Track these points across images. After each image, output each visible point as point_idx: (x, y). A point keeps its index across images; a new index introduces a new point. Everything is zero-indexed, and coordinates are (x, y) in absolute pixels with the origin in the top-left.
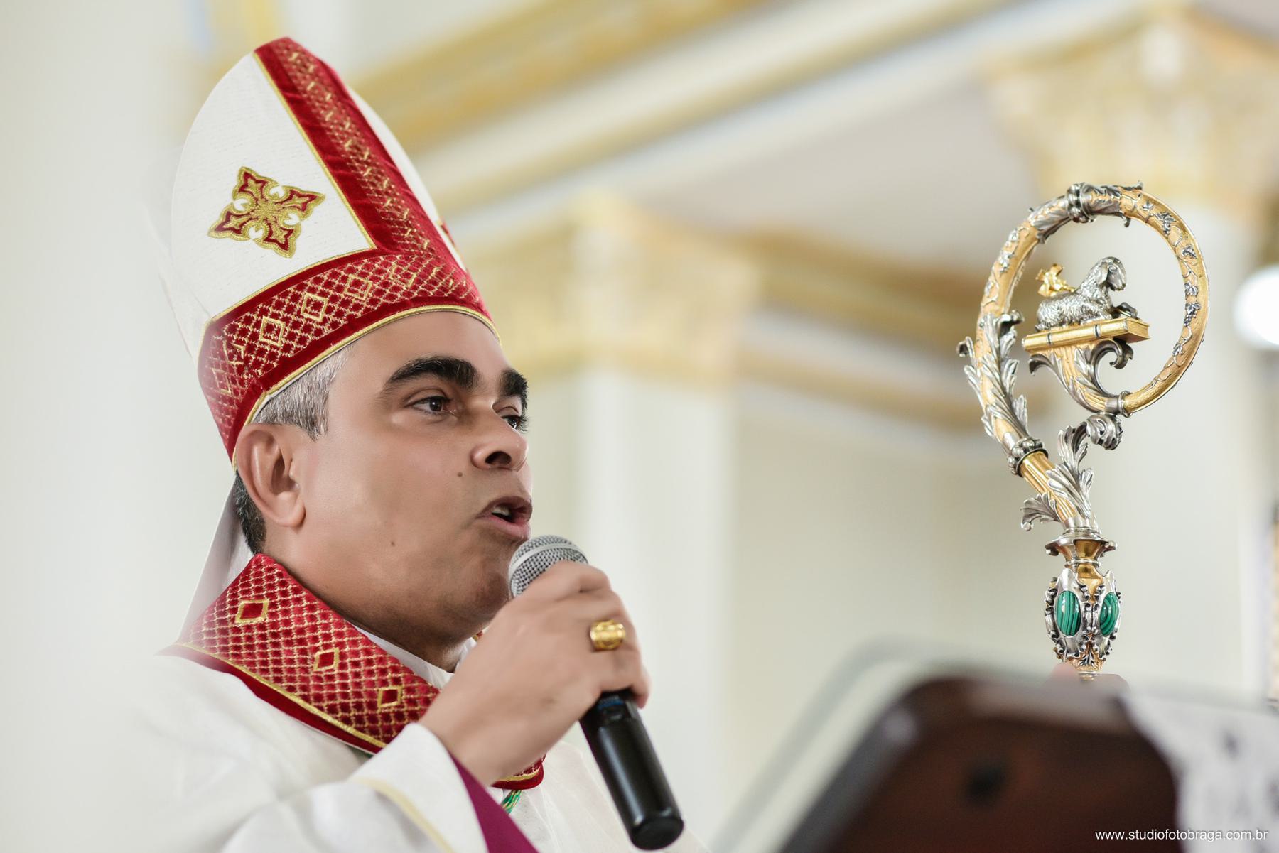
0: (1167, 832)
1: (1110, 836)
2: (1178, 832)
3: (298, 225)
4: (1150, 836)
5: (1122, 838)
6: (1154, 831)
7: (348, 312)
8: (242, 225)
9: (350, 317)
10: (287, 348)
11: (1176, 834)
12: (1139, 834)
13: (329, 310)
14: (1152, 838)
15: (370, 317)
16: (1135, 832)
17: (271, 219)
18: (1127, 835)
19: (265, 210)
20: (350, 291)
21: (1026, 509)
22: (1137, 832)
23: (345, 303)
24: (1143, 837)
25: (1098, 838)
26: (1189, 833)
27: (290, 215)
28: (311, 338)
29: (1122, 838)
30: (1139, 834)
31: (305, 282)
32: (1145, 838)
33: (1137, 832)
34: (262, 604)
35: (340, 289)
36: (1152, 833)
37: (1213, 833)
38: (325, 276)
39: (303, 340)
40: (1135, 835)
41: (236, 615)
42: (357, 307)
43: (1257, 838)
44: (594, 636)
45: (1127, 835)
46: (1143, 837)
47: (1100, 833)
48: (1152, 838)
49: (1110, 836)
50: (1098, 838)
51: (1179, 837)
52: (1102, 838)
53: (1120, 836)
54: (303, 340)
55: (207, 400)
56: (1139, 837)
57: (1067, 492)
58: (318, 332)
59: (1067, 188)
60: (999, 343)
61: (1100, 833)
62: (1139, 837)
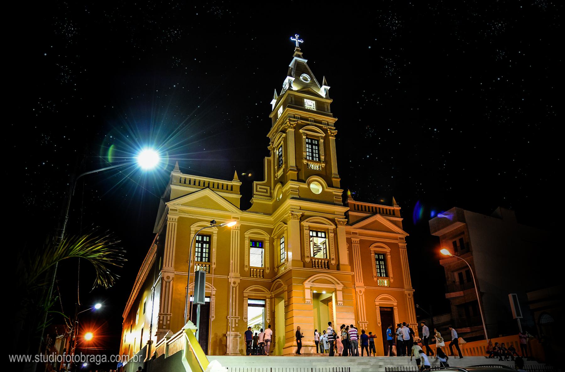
0: (64, 355)
1: (20, 359)
6: (55, 354)
12: (42, 357)
16: (39, 355)
18: (33, 358)
21: (392, 368)
22: (41, 355)
25: (11, 361)
29: (29, 361)
30: (42, 357)
33: (41, 355)
34: (462, 272)
36: (53, 356)
40: (40, 358)
41: (59, 244)
45: (33, 358)
47: (13, 356)
49: (20, 359)
50: (11, 361)
51: (74, 360)
55: (416, 307)
56: (42, 360)
57: (210, 267)
60: (304, 354)
61: (13, 356)
62: (42, 360)
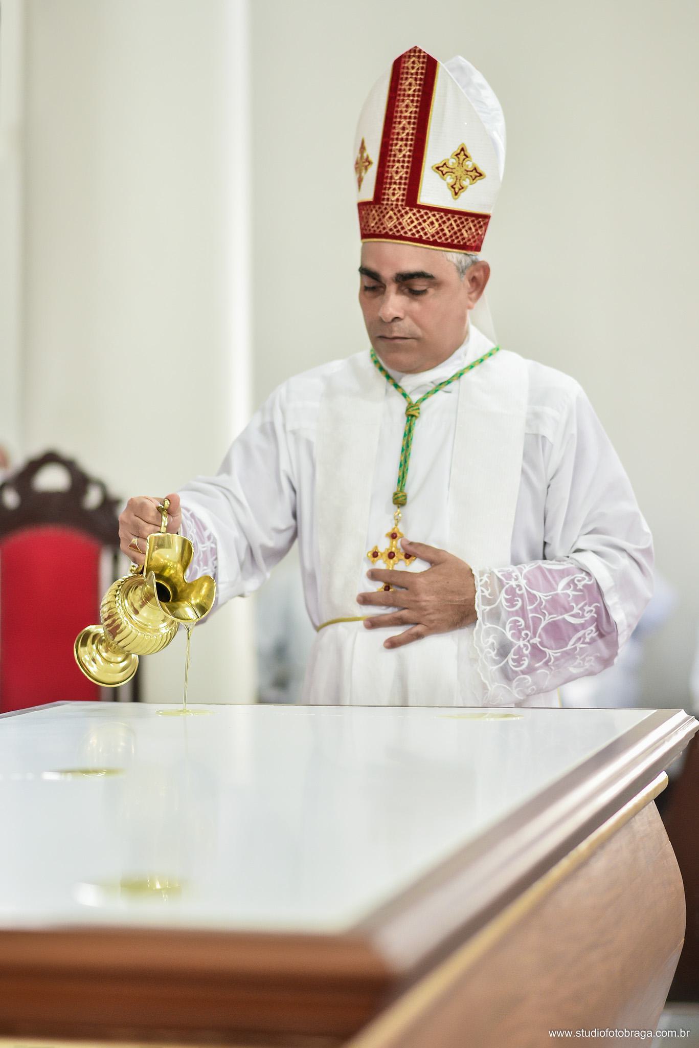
0: (607, 1031)
2: (616, 1031)
3: (467, 186)
4: (594, 1034)
5: (570, 1036)
7: (422, 233)
8: (472, 171)
9: (421, 236)
10: (391, 230)
11: (615, 1032)
13: (415, 227)
14: (595, 1036)
15: (427, 242)
17: (459, 178)
18: (574, 1034)
19: (459, 172)
20: (428, 225)
22: (583, 1031)
23: (423, 229)
24: (587, 1035)
25: (551, 1036)
26: (625, 1032)
27: (452, 180)
28: (402, 232)
29: (570, 1036)
31: (421, 210)
32: (589, 1035)
33: (583, 1031)
35: (425, 221)
36: (595, 1032)
37: (645, 1032)
38: (423, 212)
39: (398, 231)
40: (581, 1033)
42: (426, 234)
43: (681, 1036)
44: (164, 629)
45: (574, 1034)
46: (587, 1035)
48: (595, 1036)
50: (551, 1036)
52: (554, 1036)
53: (569, 1034)
54: (398, 231)
56: (584, 1035)
58: (406, 233)
59: (371, 549)
62: (584, 1035)
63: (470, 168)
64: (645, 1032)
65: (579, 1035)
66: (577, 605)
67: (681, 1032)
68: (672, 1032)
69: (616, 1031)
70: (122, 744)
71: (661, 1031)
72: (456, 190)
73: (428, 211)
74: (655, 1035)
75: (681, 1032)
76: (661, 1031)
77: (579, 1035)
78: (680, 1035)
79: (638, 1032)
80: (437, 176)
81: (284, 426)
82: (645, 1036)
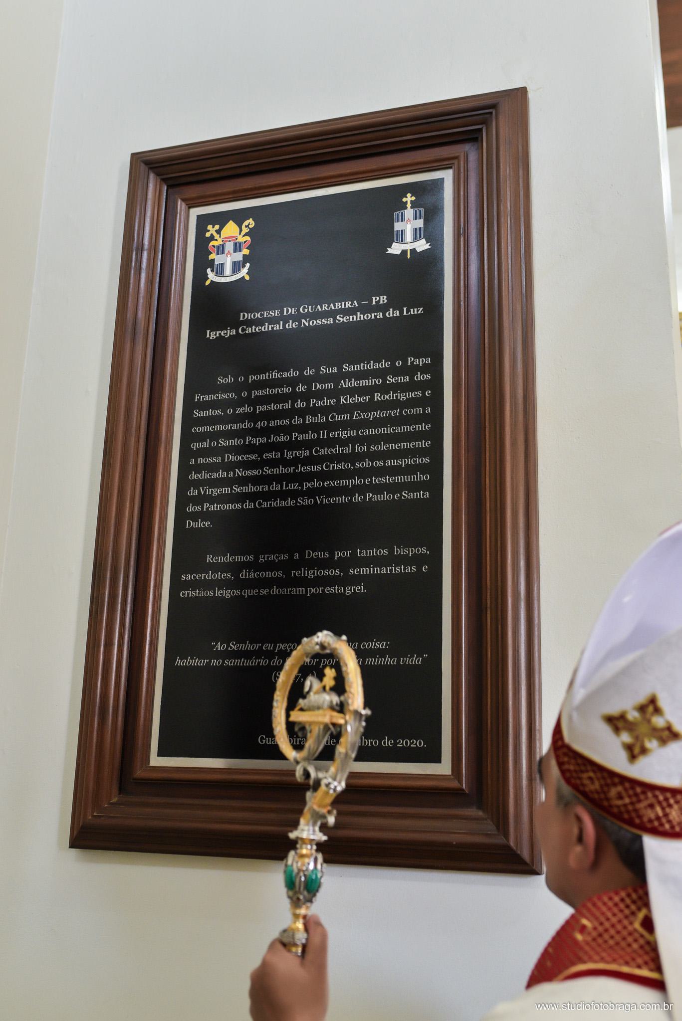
22: (568, 1005)
36: (581, 1005)
37: (629, 1005)
43: (665, 1009)
63: (648, 745)
64: (629, 1005)
65: (565, 1008)
66: (363, 754)
67: (665, 1005)
68: (656, 1005)
69: (601, 1005)
70: (604, 947)
71: (645, 1005)
72: (634, 752)
73: (321, 652)
74: (639, 1008)
75: (665, 1005)
76: (645, 1005)
77: (564, 1008)
78: (663, 1009)
79: (634, 1006)
80: (642, 761)
81: (487, 835)
82: (629, 1009)
